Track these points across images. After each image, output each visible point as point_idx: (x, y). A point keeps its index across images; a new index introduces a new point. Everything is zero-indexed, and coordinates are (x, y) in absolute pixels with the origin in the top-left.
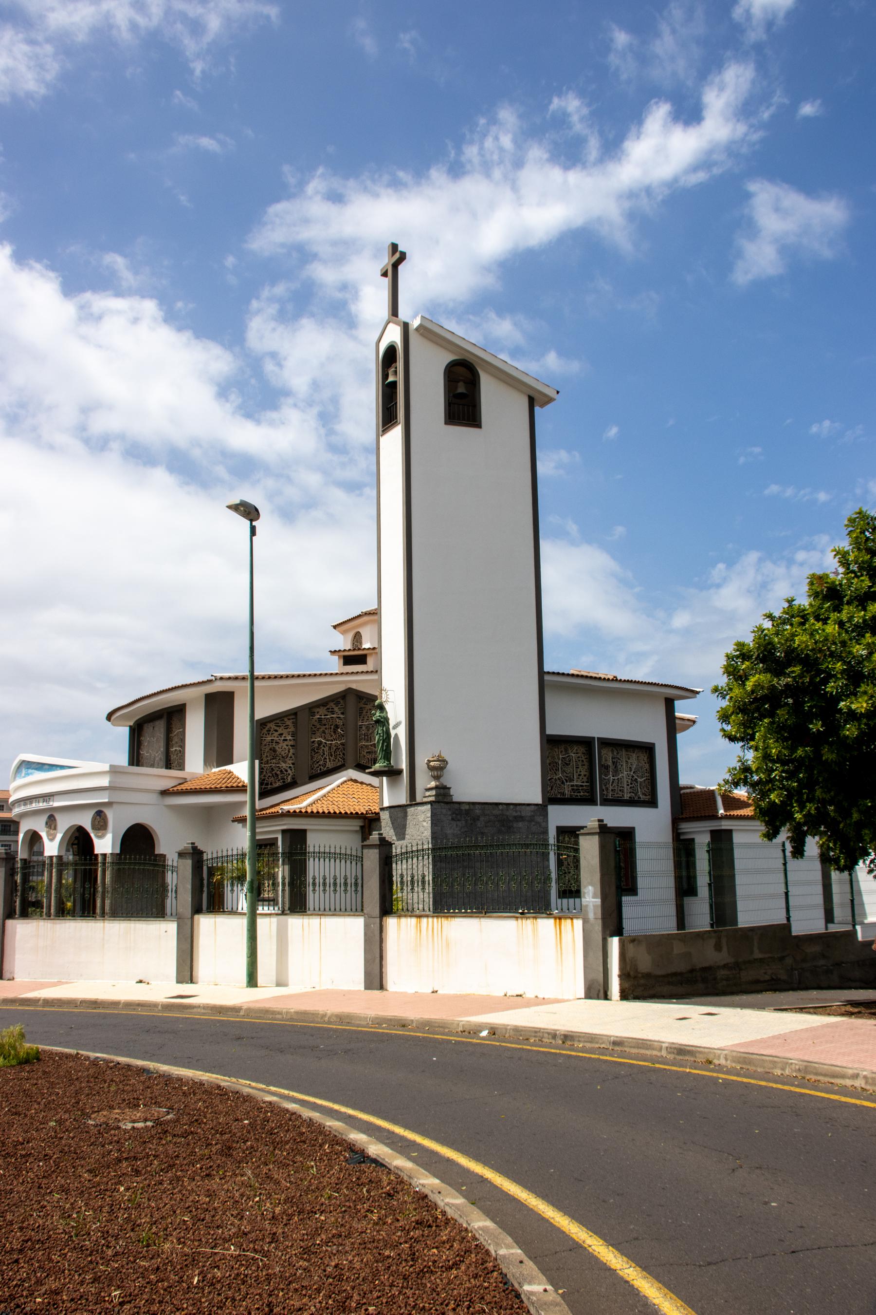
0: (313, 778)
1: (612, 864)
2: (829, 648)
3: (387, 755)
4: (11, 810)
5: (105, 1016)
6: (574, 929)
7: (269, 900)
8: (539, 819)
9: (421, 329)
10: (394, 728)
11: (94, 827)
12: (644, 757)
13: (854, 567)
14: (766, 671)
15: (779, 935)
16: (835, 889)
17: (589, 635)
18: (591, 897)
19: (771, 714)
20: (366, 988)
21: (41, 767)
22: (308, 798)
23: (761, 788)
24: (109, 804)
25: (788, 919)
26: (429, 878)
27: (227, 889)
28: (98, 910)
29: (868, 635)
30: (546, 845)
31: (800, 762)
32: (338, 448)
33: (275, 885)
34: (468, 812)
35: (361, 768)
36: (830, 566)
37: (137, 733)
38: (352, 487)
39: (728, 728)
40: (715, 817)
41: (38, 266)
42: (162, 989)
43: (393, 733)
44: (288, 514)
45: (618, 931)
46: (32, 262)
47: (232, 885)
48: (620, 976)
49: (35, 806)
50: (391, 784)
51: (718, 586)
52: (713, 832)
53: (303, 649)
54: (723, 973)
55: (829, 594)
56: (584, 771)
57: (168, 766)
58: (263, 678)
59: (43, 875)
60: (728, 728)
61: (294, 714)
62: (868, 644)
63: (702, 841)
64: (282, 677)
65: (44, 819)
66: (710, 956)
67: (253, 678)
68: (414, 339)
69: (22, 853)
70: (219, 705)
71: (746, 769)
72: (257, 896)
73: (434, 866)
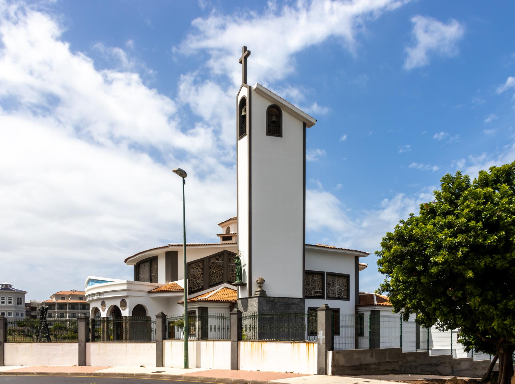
0: (211, 286)
1: (330, 322)
2: (428, 235)
3: (240, 277)
4: (86, 299)
5: (128, 380)
6: (314, 348)
7: (193, 335)
8: (301, 304)
9: (257, 89)
10: (243, 266)
11: (121, 306)
12: (345, 280)
13: (443, 200)
14: (399, 245)
15: (397, 352)
16: (421, 335)
17: (326, 230)
18: (321, 335)
19: (401, 263)
20: (231, 369)
21: (98, 281)
22: (208, 294)
23: (393, 293)
24: (127, 297)
25: (401, 346)
26: (257, 326)
27: (176, 330)
28: (124, 339)
29: (446, 229)
30: (304, 314)
31: (411, 283)
32: (221, 147)
33: (195, 328)
34: (273, 301)
35: (230, 283)
36: (431, 199)
37: (138, 268)
38: (228, 165)
39: (381, 268)
40: (373, 305)
41: (82, 55)
42: (150, 368)
43: (243, 268)
44: (202, 176)
45: (332, 349)
46: (79, 53)
47: (178, 329)
48: (332, 366)
49: (96, 297)
50: (242, 289)
51: (384, 209)
52: (371, 311)
53: (206, 233)
54: (374, 366)
55: (429, 212)
56: (320, 285)
57: (151, 281)
58: (190, 245)
59: (100, 325)
60: (381, 268)
61: (202, 260)
62: (445, 233)
63: (367, 314)
64: (197, 245)
65: (100, 302)
66: (369, 359)
67: (186, 245)
68: (253, 94)
69: (91, 317)
70: (171, 257)
71: (388, 285)
72: (188, 333)
73: (259, 322)
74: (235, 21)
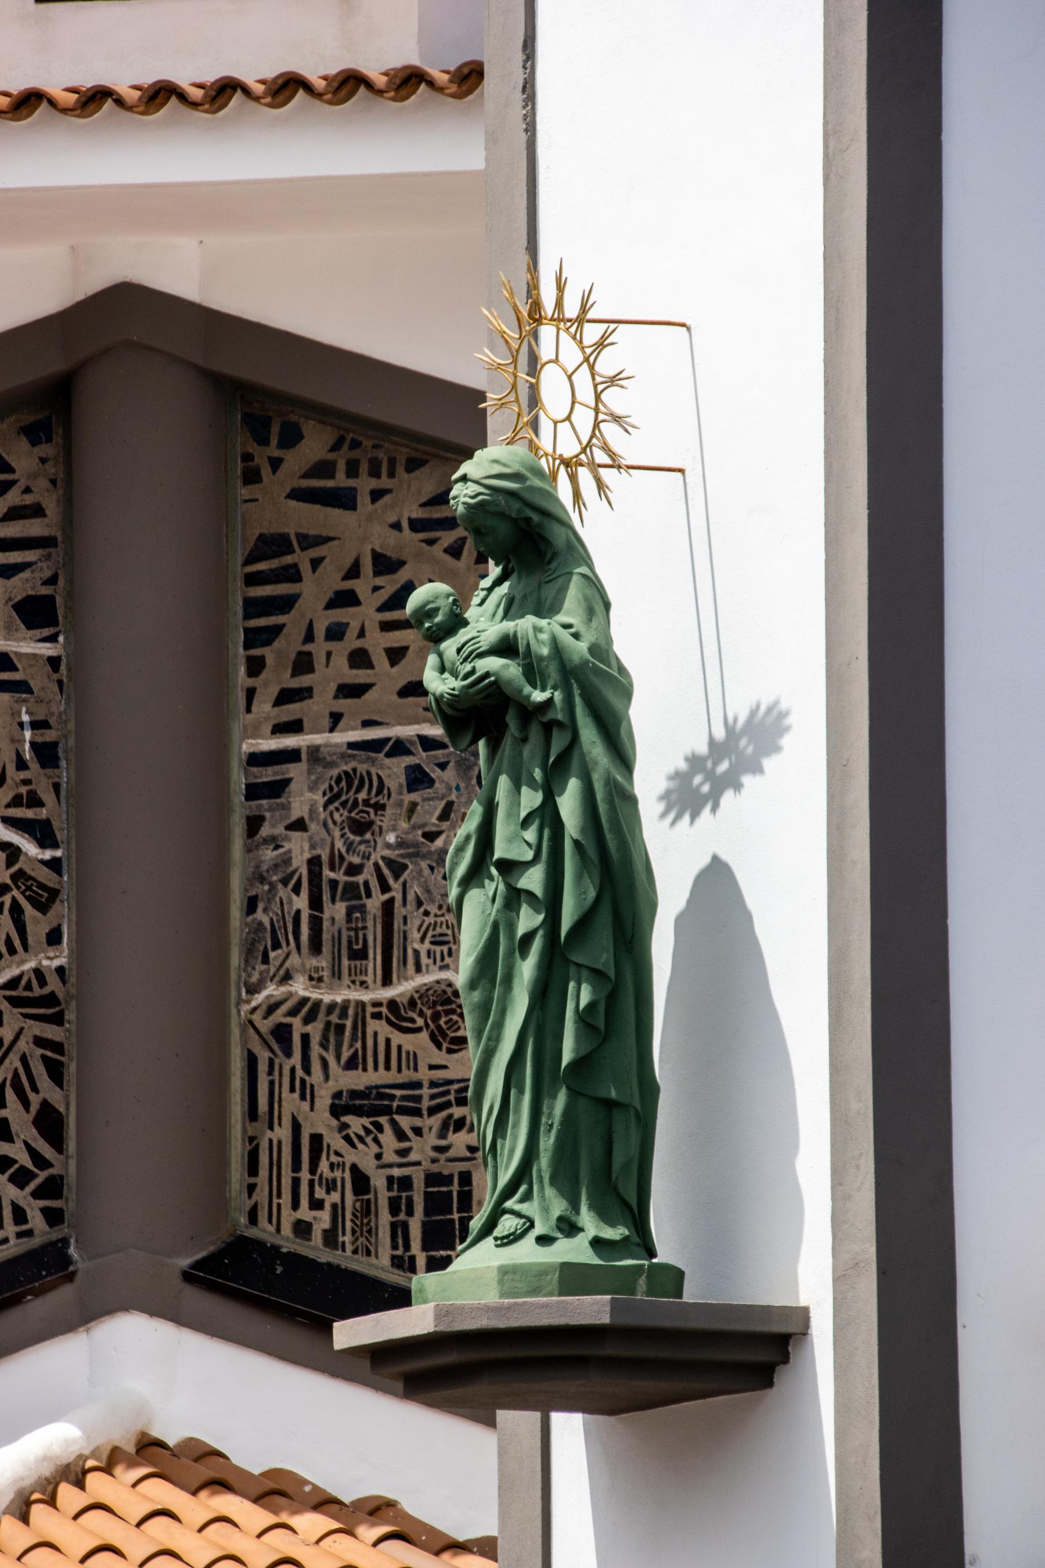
35: (272, 1291)
43: (672, 855)
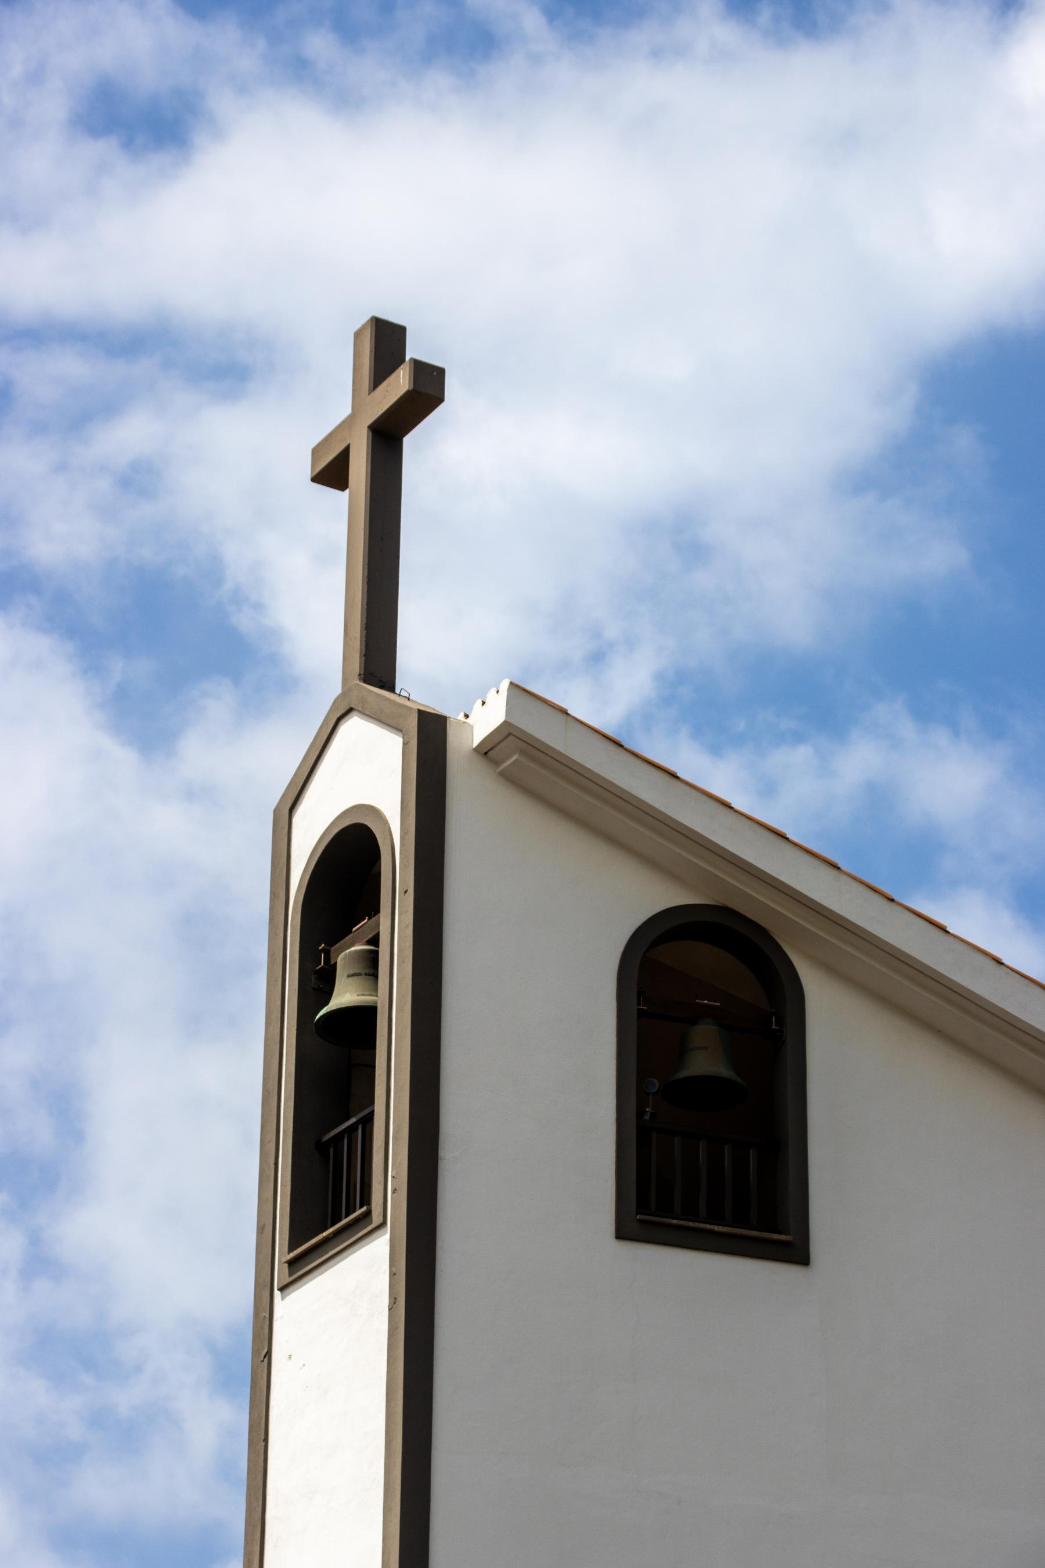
68: (469, 794)
74: (299, 72)
